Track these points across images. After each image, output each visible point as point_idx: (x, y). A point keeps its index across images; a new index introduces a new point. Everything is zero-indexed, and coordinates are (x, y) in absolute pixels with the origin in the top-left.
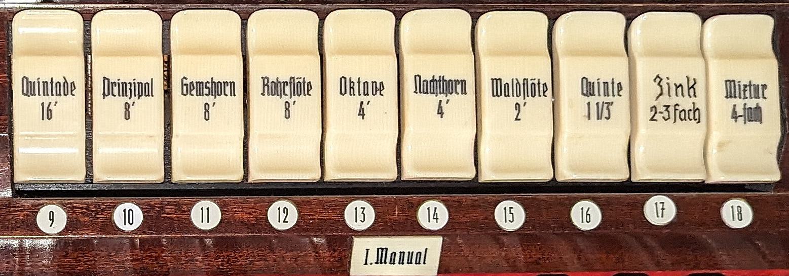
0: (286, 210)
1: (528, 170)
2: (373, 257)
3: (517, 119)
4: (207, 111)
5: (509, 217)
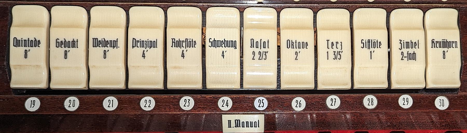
1: (220, 83)
2: (233, 124)
3: (253, 59)
4: (444, 54)
5: (262, 104)
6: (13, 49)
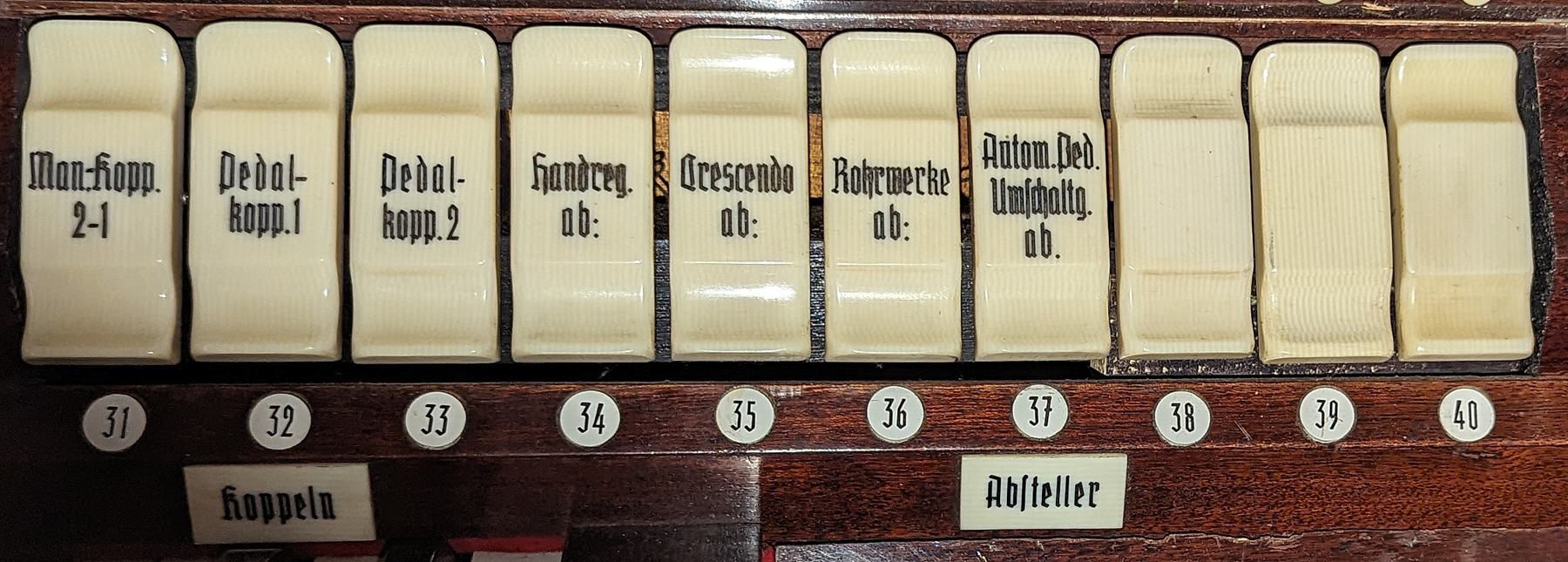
1: (556, 337)
5: (747, 420)
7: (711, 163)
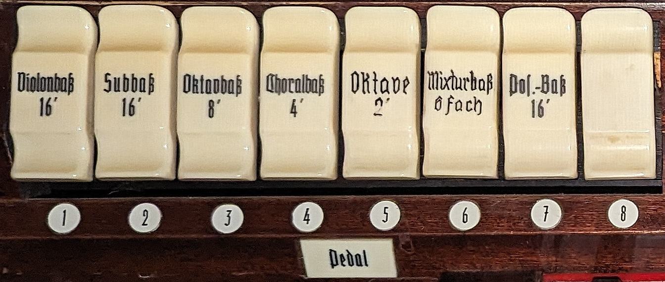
0: (146, 212)
1: (222, 170)
6: (15, 94)
7: (295, 78)
